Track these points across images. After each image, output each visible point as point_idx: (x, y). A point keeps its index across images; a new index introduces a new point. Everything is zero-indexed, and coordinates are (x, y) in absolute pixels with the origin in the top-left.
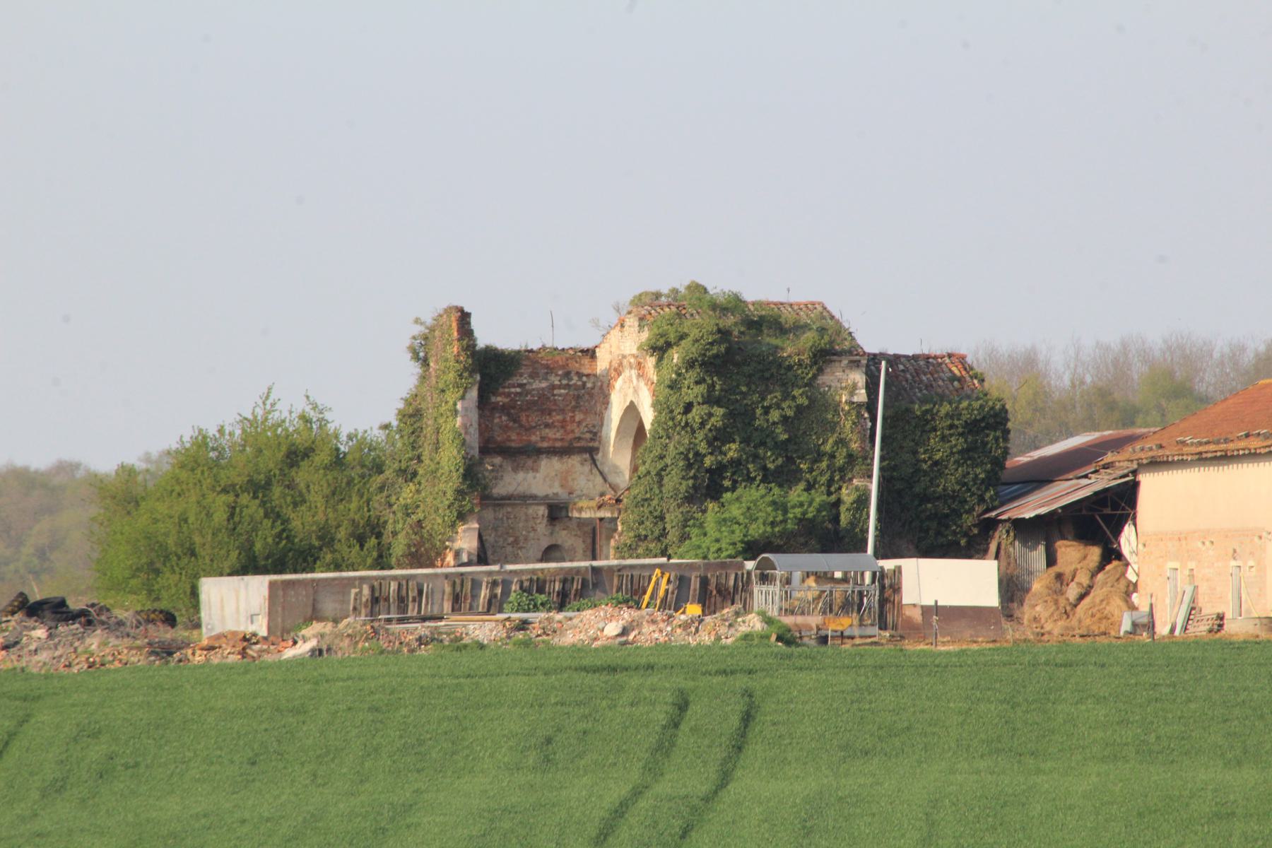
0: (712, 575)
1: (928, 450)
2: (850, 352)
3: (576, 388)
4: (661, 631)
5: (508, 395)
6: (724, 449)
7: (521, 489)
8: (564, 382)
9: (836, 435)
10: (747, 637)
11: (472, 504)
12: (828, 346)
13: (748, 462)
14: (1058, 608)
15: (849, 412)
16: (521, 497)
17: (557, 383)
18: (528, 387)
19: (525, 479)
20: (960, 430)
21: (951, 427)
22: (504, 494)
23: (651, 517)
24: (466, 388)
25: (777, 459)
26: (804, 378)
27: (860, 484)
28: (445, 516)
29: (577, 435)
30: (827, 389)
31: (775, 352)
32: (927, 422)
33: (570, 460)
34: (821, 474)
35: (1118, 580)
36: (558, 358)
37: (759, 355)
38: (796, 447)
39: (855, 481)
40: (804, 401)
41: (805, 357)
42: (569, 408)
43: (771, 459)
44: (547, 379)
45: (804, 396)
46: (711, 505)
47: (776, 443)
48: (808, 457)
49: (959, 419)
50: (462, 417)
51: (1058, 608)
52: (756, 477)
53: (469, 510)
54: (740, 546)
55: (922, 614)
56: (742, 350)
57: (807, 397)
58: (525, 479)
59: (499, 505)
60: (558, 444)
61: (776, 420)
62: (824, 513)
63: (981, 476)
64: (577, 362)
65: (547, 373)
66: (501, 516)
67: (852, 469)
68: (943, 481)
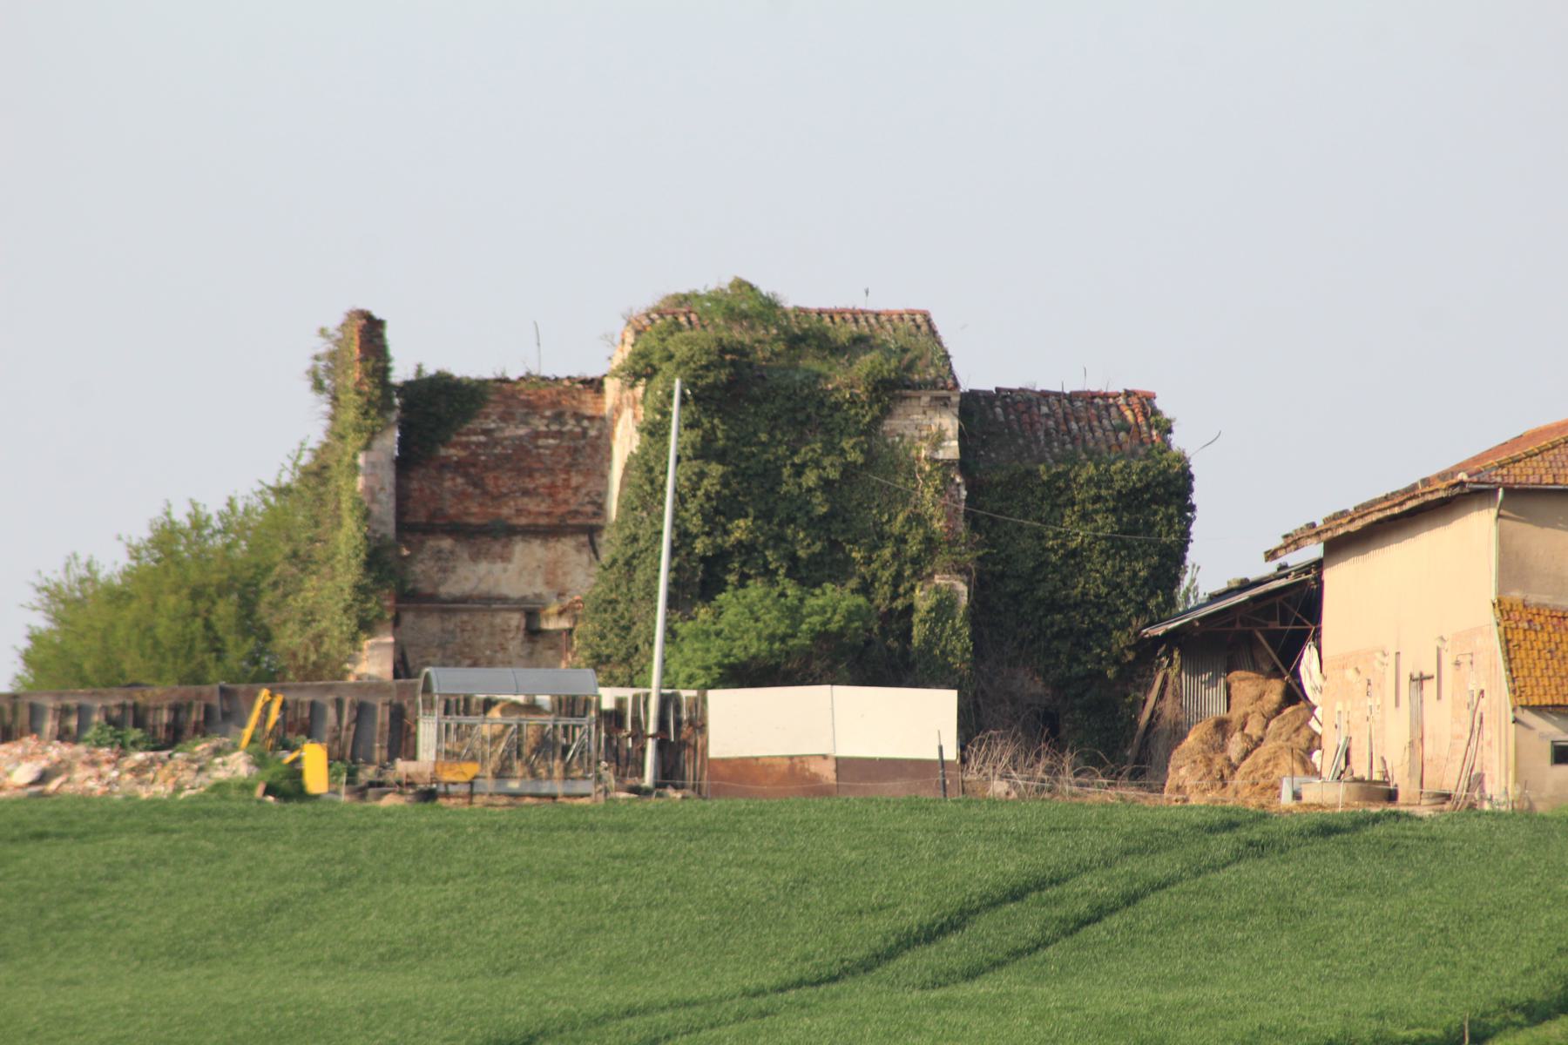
1: (1060, 533)
5: (466, 446)
6: (730, 526)
8: (554, 428)
9: (911, 508)
10: (219, 787)
11: (382, 607)
12: (893, 374)
13: (766, 547)
14: (1210, 772)
15: (930, 475)
17: (543, 428)
18: (497, 435)
19: (490, 572)
20: (1111, 504)
21: (1097, 499)
23: (616, 630)
25: (814, 543)
27: (943, 582)
29: (573, 507)
30: (897, 439)
31: (815, 382)
32: (1061, 491)
33: (559, 546)
34: (884, 567)
35: (1297, 730)
36: (544, 392)
38: (843, 526)
40: (855, 457)
43: (805, 543)
44: (527, 423)
46: (702, 611)
47: (811, 519)
49: (1108, 488)
50: (365, 475)
51: (1210, 772)
52: (777, 569)
53: (376, 616)
54: (716, 671)
55: (837, 771)
57: (862, 451)
58: (490, 572)
60: (543, 521)
61: (811, 484)
62: (857, 624)
63: (1142, 574)
64: (574, 398)
65: (527, 414)
67: (933, 559)
68: (1082, 581)
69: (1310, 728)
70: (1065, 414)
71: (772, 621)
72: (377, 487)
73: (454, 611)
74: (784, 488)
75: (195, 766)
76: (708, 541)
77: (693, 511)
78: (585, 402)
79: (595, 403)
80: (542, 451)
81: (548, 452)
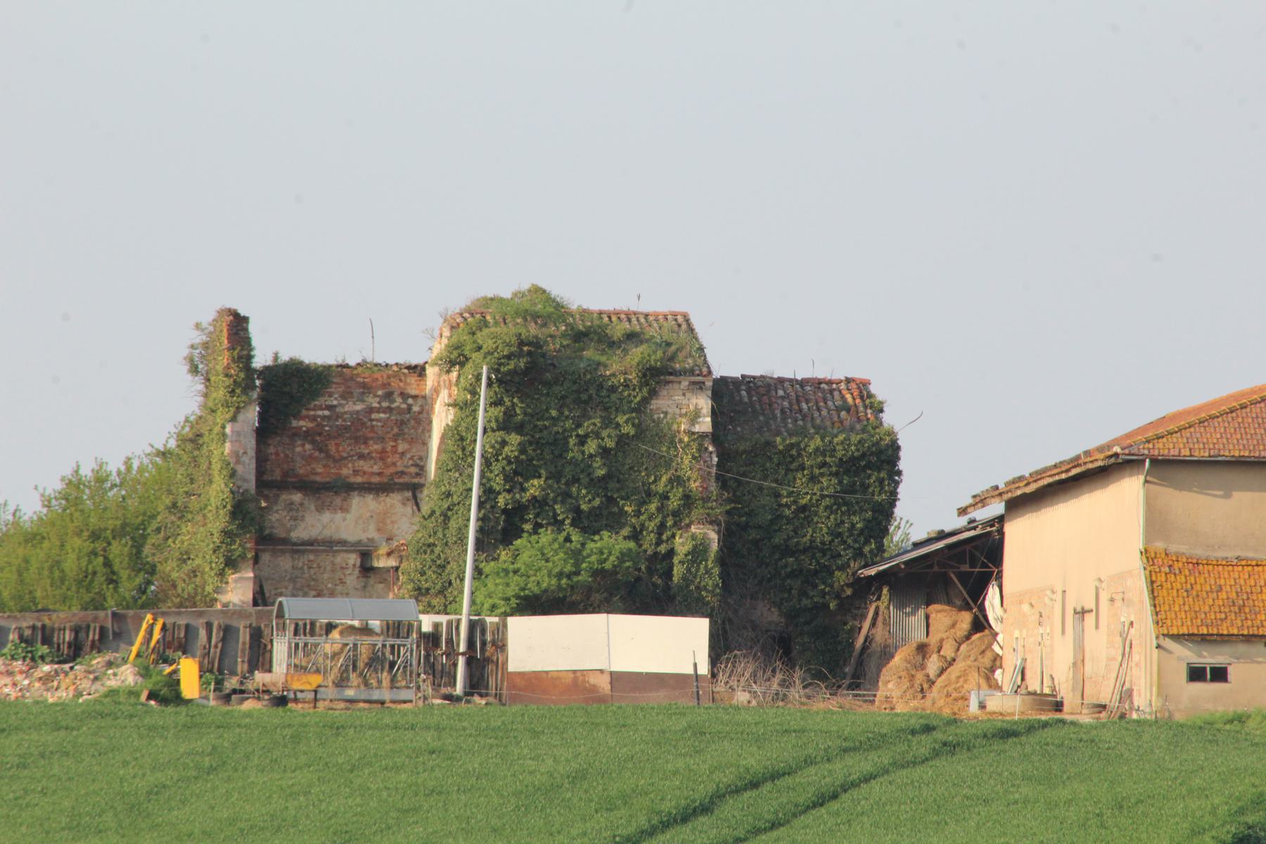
0: (265, 625)
2: (691, 372)
3: (400, 411)
4: (15, 685)
5: (314, 419)
7: (327, 533)
8: (385, 404)
10: (112, 693)
11: (244, 549)
12: (659, 363)
13: (555, 502)
14: (912, 686)
15: (688, 445)
16: (327, 542)
17: (375, 405)
18: (338, 410)
21: (824, 464)
22: (306, 539)
23: (434, 568)
24: (238, 408)
25: (594, 499)
26: (632, 401)
28: (211, 562)
29: (400, 469)
30: (662, 416)
31: (596, 370)
32: (793, 459)
33: (388, 499)
34: (650, 519)
35: (983, 652)
36: (377, 375)
37: (574, 372)
39: (693, 529)
40: (628, 429)
41: (633, 377)
42: (390, 436)
43: (587, 499)
44: (363, 401)
45: (630, 424)
46: (503, 553)
47: (592, 480)
48: (633, 498)
49: (831, 456)
50: (231, 442)
51: (912, 686)
52: (564, 520)
53: (239, 556)
54: (514, 602)
56: (554, 366)
57: (633, 425)
59: (297, 551)
60: (376, 479)
61: (592, 451)
62: (628, 564)
64: (401, 380)
66: (301, 565)
68: (810, 530)
69: (993, 650)
70: (797, 396)
71: (560, 561)
72: (241, 452)
73: (304, 552)
74: (570, 455)
75: (91, 676)
76: (508, 497)
77: (496, 473)
78: (410, 384)
79: (418, 385)
80: (374, 423)
81: (379, 424)
